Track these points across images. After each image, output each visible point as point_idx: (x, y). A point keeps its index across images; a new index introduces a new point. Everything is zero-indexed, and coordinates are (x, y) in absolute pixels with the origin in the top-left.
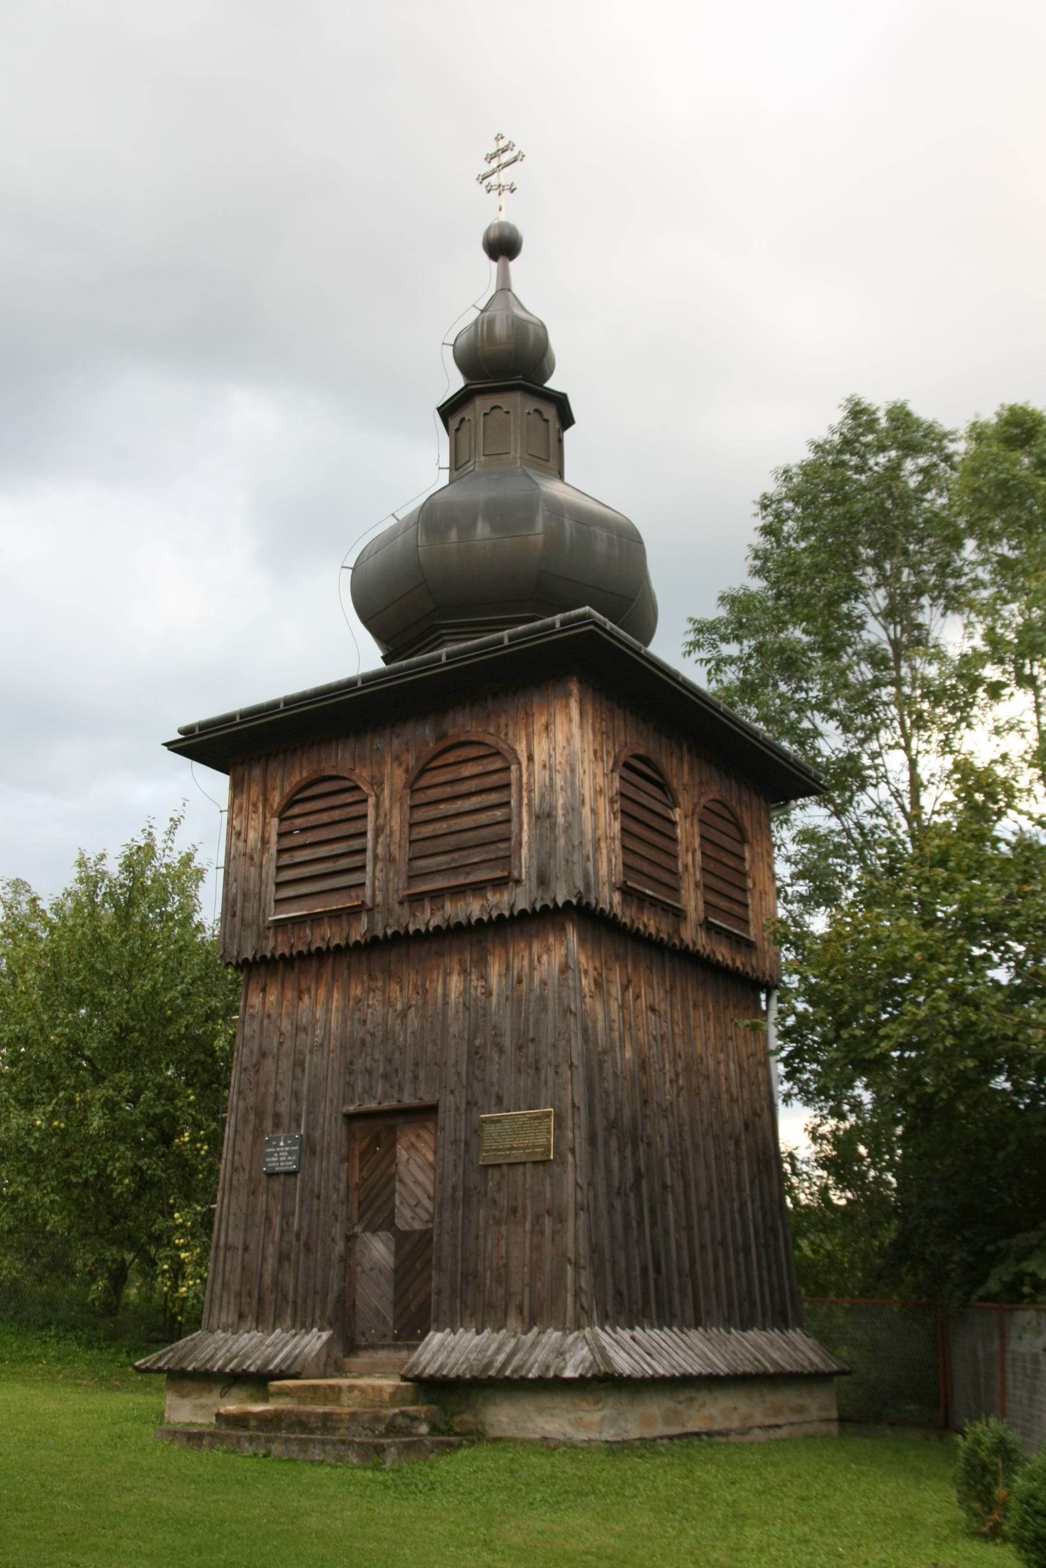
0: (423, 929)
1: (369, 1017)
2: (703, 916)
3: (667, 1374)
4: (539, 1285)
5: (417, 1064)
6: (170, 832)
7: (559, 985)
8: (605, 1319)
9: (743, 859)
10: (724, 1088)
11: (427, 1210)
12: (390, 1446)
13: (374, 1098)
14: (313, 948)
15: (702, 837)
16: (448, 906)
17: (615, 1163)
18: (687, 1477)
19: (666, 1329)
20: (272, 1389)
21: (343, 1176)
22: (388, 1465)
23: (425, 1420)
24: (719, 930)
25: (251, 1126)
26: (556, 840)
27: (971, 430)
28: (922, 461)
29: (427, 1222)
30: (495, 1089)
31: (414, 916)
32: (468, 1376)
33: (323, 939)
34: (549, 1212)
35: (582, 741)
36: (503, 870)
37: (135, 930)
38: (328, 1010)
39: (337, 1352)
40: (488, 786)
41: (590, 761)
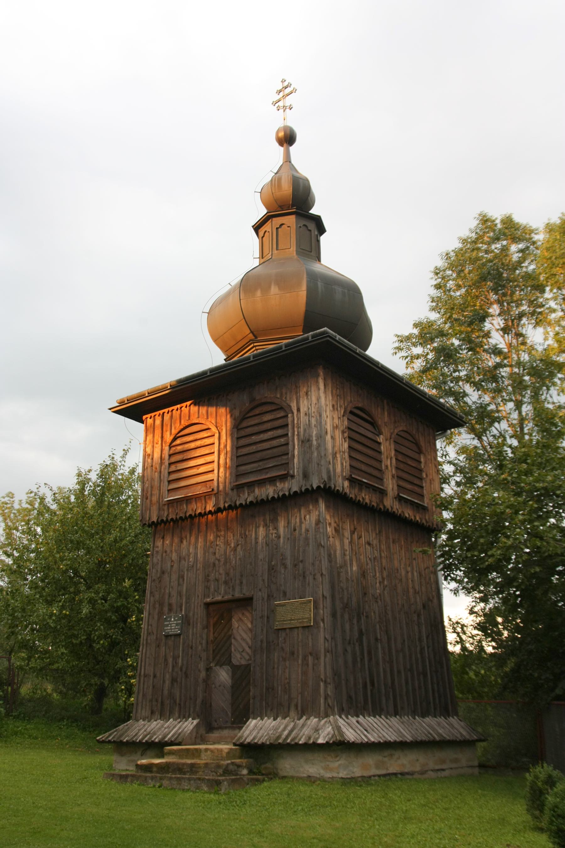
0: (244, 503)
1: (217, 551)
2: (397, 493)
3: (376, 741)
4: (306, 693)
5: (242, 576)
6: (123, 457)
7: (315, 532)
8: (342, 711)
9: (420, 462)
10: (411, 586)
11: (248, 654)
12: (223, 781)
13: (220, 594)
14: (188, 515)
15: (396, 450)
16: (257, 491)
17: (347, 626)
18: (383, 797)
19: (377, 717)
20: (166, 751)
21: (205, 636)
22: (223, 791)
23: (245, 767)
24: (406, 501)
25: (157, 611)
26: (312, 453)
27: (546, 227)
28: (521, 246)
29: (248, 660)
30: (282, 588)
31: (239, 496)
32: (268, 743)
33: (192, 510)
34: (311, 654)
35: (326, 400)
36: (285, 470)
37: (105, 508)
38: (196, 548)
39: (202, 731)
40: (277, 426)
41: (330, 411)
